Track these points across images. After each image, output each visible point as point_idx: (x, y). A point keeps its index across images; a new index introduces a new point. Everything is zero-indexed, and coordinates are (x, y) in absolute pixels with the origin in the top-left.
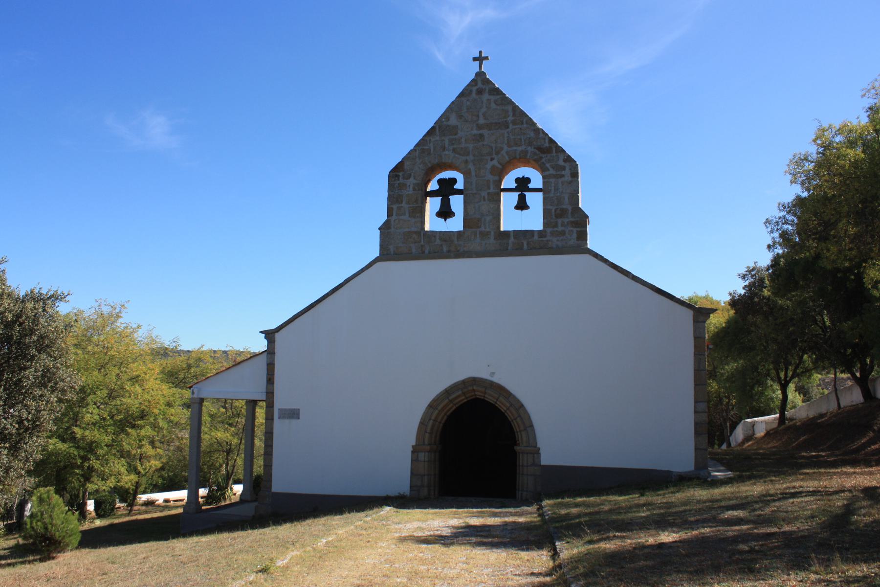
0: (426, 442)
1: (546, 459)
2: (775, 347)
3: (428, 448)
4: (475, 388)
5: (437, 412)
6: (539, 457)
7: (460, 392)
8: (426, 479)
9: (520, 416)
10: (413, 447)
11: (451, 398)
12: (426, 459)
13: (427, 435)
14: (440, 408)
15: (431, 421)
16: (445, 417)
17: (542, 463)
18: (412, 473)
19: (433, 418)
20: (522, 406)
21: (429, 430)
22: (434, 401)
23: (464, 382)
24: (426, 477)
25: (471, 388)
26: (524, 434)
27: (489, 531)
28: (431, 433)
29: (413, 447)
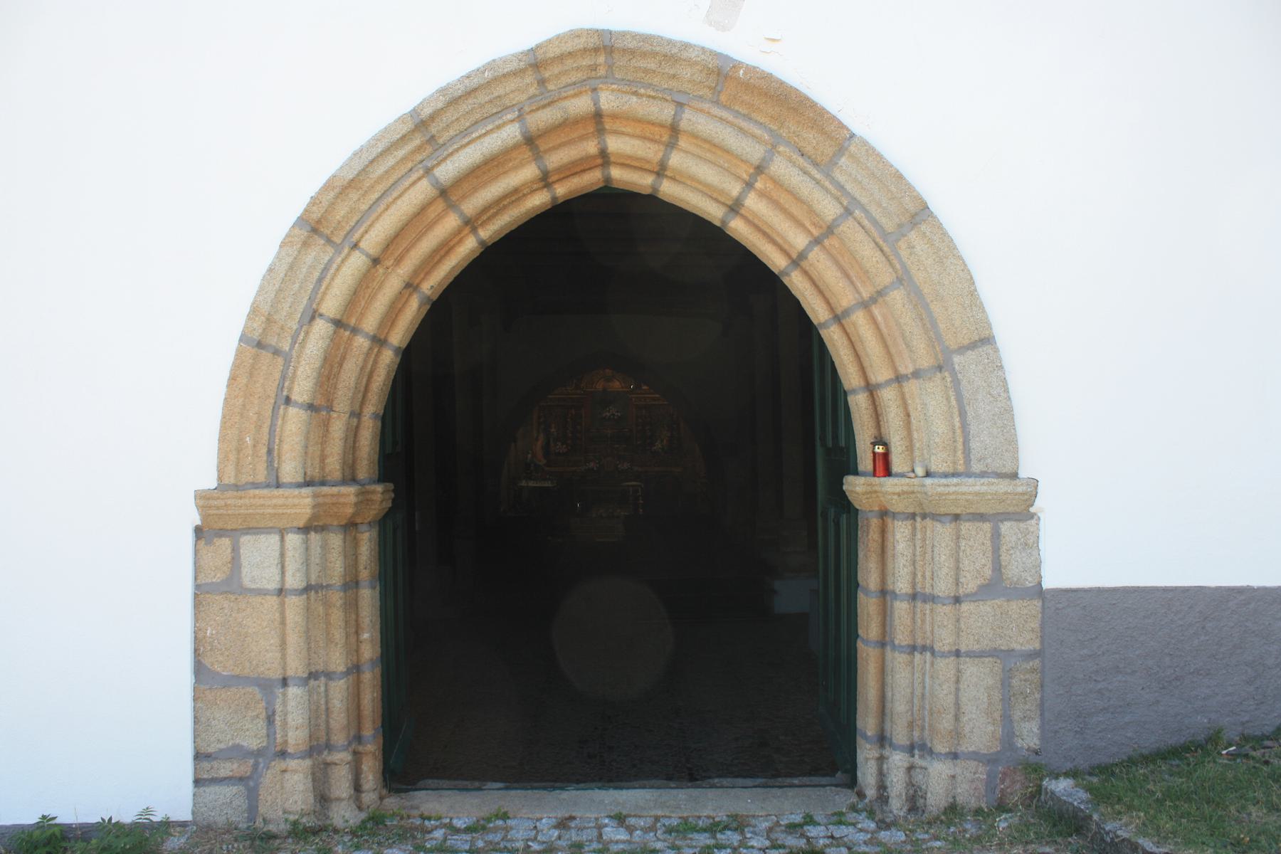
0: (290, 469)
1: (1076, 553)
2: (290, 840)
3: (302, 503)
4: (608, 100)
5: (357, 262)
6: (1031, 545)
7: (511, 133)
8: (294, 703)
9: (904, 279)
10: (203, 499)
11: (447, 171)
12: (294, 580)
13: (294, 422)
14: (373, 239)
15: (321, 329)
16: (412, 312)
17: (1051, 581)
18: (200, 669)
19: (331, 305)
20: (920, 214)
21: (302, 389)
22: (343, 188)
23: (537, 64)
24: (294, 691)
25: (580, 105)
26: (930, 401)
27: (841, 150)
28: (318, 408)
29: (203, 499)
